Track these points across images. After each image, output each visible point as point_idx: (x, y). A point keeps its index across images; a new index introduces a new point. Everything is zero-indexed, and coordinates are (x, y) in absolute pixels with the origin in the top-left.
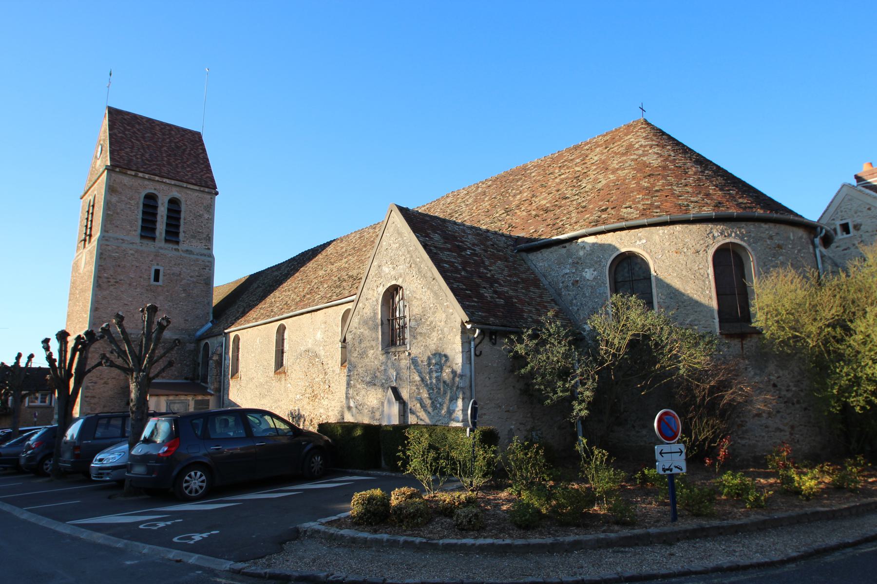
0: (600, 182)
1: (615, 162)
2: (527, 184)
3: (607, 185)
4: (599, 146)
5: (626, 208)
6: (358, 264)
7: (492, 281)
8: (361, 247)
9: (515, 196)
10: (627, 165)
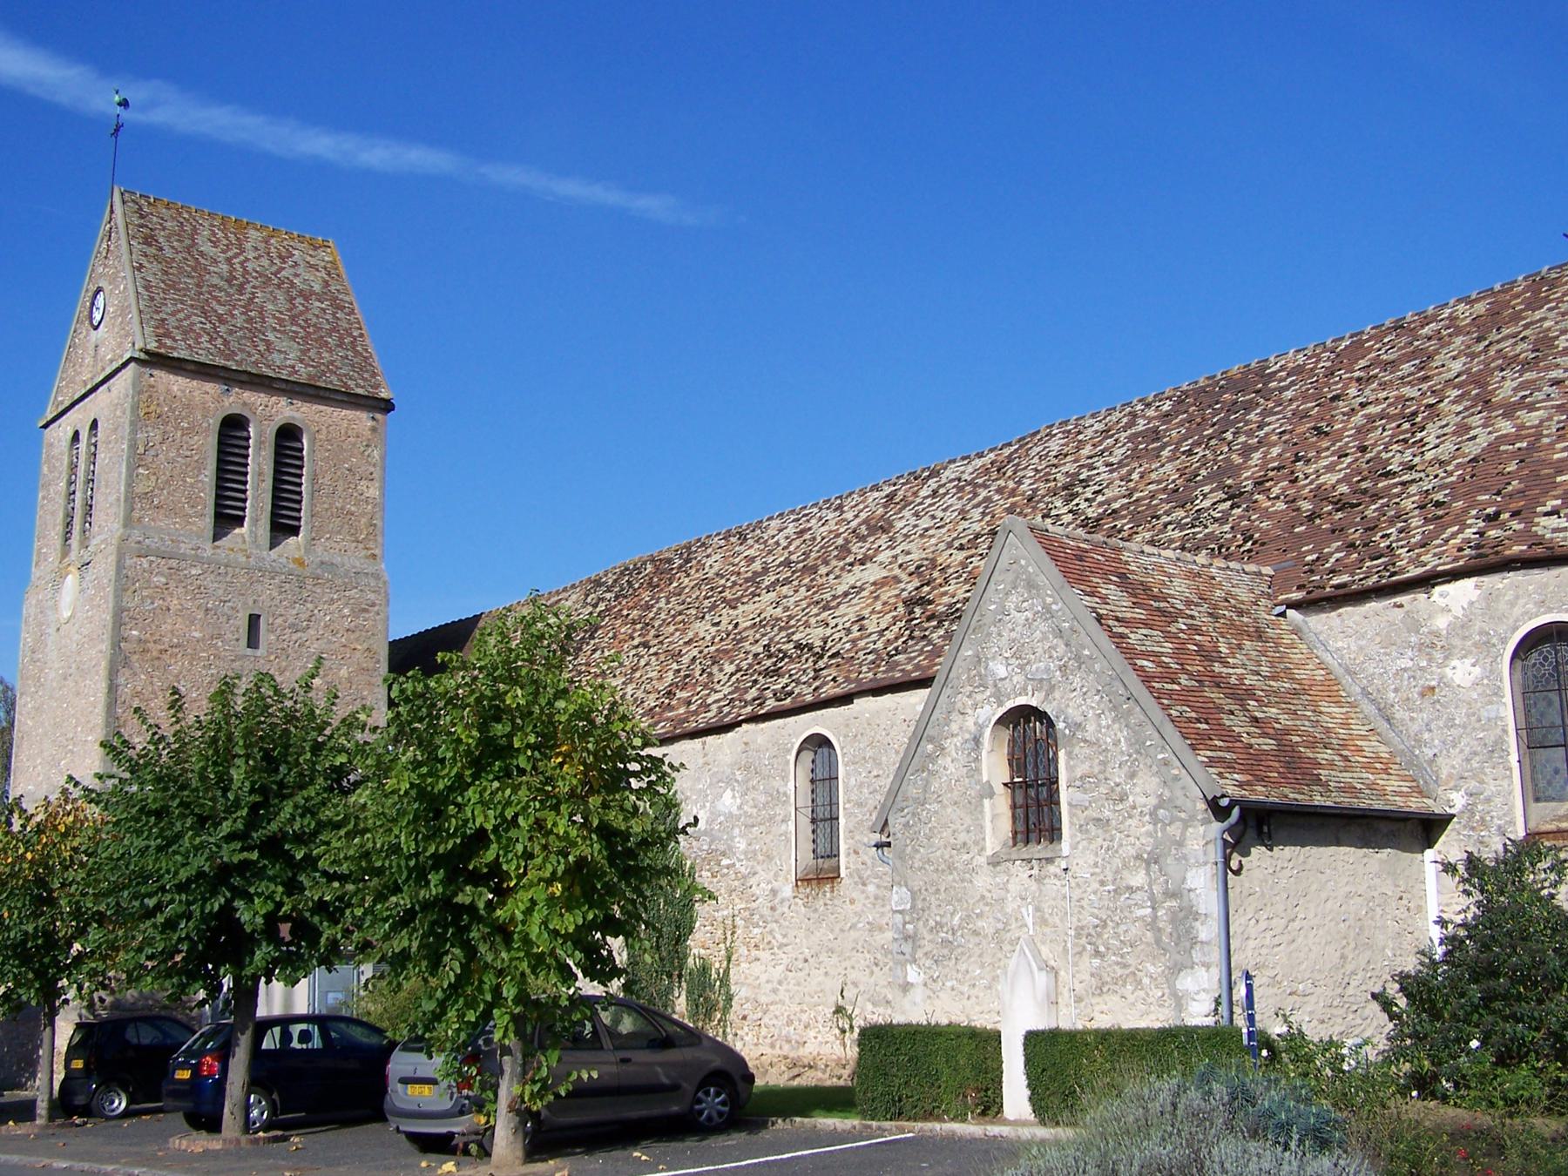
0: (1474, 438)
1: (1508, 384)
2: (1275, 424)
3: (1493, 447)
4: (1459, 331)
5: (1547, 514)
6: (815, 611)
7: (1241, 695)
8: (810, 561)
9: (1247, 451)
10: (1539, 395)
